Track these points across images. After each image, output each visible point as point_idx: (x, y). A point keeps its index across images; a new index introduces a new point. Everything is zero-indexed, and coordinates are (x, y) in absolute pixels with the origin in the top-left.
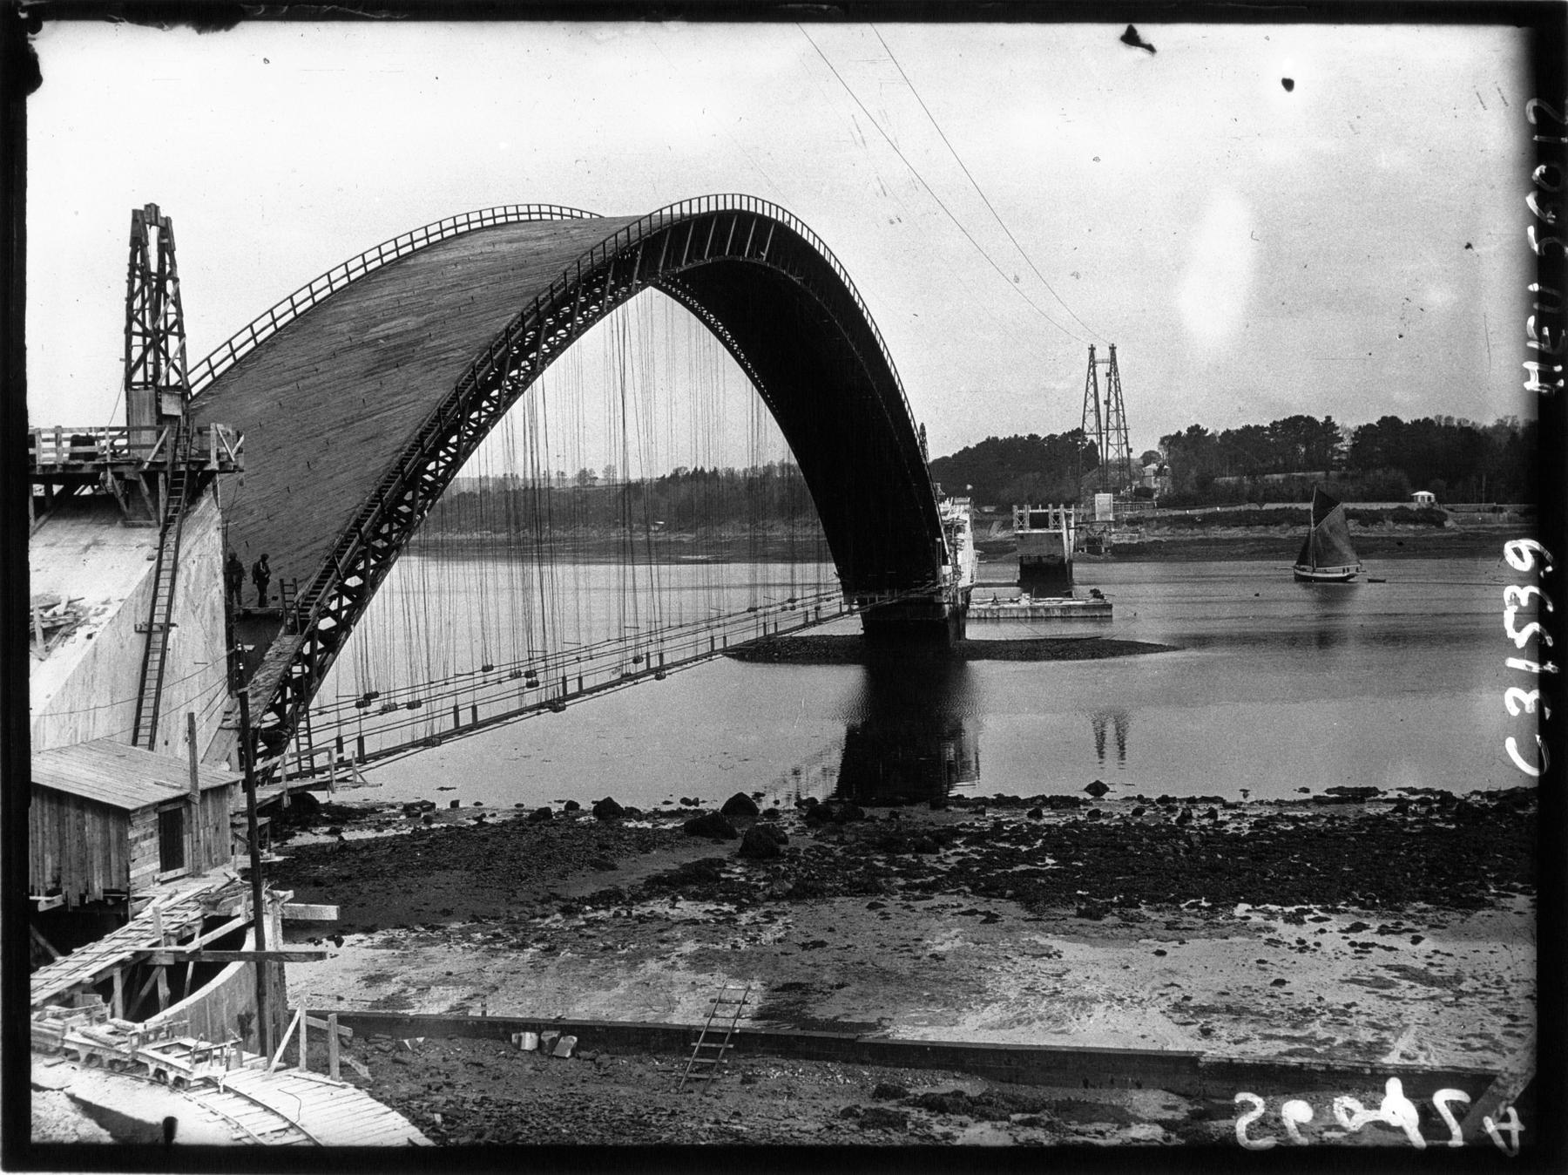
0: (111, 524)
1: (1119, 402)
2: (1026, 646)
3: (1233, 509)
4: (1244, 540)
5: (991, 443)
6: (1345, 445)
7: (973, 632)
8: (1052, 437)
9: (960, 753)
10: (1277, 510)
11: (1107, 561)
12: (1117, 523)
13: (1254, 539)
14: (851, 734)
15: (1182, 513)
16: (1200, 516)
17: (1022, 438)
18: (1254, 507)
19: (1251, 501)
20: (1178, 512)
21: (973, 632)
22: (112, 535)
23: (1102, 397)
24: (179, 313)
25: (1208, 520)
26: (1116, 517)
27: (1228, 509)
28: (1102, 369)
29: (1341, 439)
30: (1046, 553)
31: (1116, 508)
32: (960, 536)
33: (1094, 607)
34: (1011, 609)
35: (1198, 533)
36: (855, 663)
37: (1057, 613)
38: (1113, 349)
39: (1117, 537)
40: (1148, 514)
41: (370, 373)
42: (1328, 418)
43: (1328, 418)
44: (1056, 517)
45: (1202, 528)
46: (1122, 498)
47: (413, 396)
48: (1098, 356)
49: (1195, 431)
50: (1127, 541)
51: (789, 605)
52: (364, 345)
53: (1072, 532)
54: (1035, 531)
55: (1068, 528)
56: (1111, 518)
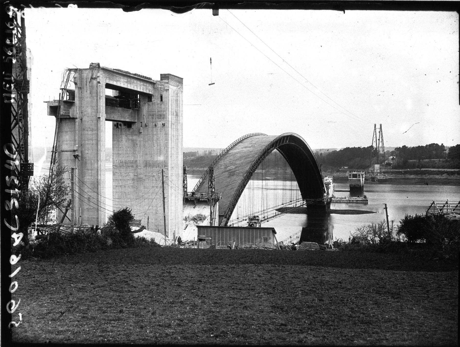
0: (206, 205)
1: (382, 140)
2: (343, 211)
3: (413, 170)
4: (415, 179)
5: (348, 149)
6: (447, 151)
7: (332, 207)
8: (364, 148)
9: (328, 234)
10: (425, 170)
11: (376, 184)
12: (380, 173)
13: (418, 179)
14: (303, 229)
15: (399, 170)
16: (403, 171)
17: (356, 148)
18: (419, 169)
19: (418, 168)
20: (397, 170)
21: (332, 207)
22: (206, 206)
23: (378, 138)
24: (23, 34)
25: (406, 173)
26: (380, 171)
27: (411, 170)
28: (378, 130)
29: (446, 150)
30: (356, 184)
31: (380, 169)
32: (330, 185)
33: (364, 200)
34: (344, 200)
35: (403, 176)
36: (304, 213)
37: (355, 201)
38: (381, 125)
39: (380, 177)
40: (389, 170)
41: (229, 177)
42: (442, 144)
43: (442, 144)
44: (359, 175)
45: (404, 175)
46: (383, 166)
47: (236, 182)
48: (377, 127)
49: (404, 147)
50: (382, 178)
51: (290, 203)
52: (227, 171)
53: (364, 179)
54: (354, 179)
55: (362, 178)
56: (379, 171)
